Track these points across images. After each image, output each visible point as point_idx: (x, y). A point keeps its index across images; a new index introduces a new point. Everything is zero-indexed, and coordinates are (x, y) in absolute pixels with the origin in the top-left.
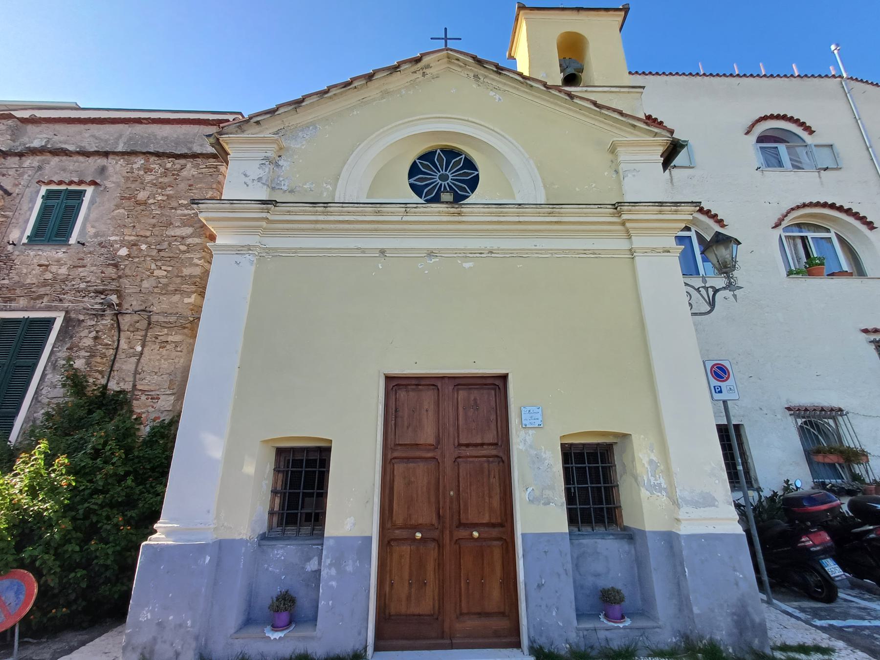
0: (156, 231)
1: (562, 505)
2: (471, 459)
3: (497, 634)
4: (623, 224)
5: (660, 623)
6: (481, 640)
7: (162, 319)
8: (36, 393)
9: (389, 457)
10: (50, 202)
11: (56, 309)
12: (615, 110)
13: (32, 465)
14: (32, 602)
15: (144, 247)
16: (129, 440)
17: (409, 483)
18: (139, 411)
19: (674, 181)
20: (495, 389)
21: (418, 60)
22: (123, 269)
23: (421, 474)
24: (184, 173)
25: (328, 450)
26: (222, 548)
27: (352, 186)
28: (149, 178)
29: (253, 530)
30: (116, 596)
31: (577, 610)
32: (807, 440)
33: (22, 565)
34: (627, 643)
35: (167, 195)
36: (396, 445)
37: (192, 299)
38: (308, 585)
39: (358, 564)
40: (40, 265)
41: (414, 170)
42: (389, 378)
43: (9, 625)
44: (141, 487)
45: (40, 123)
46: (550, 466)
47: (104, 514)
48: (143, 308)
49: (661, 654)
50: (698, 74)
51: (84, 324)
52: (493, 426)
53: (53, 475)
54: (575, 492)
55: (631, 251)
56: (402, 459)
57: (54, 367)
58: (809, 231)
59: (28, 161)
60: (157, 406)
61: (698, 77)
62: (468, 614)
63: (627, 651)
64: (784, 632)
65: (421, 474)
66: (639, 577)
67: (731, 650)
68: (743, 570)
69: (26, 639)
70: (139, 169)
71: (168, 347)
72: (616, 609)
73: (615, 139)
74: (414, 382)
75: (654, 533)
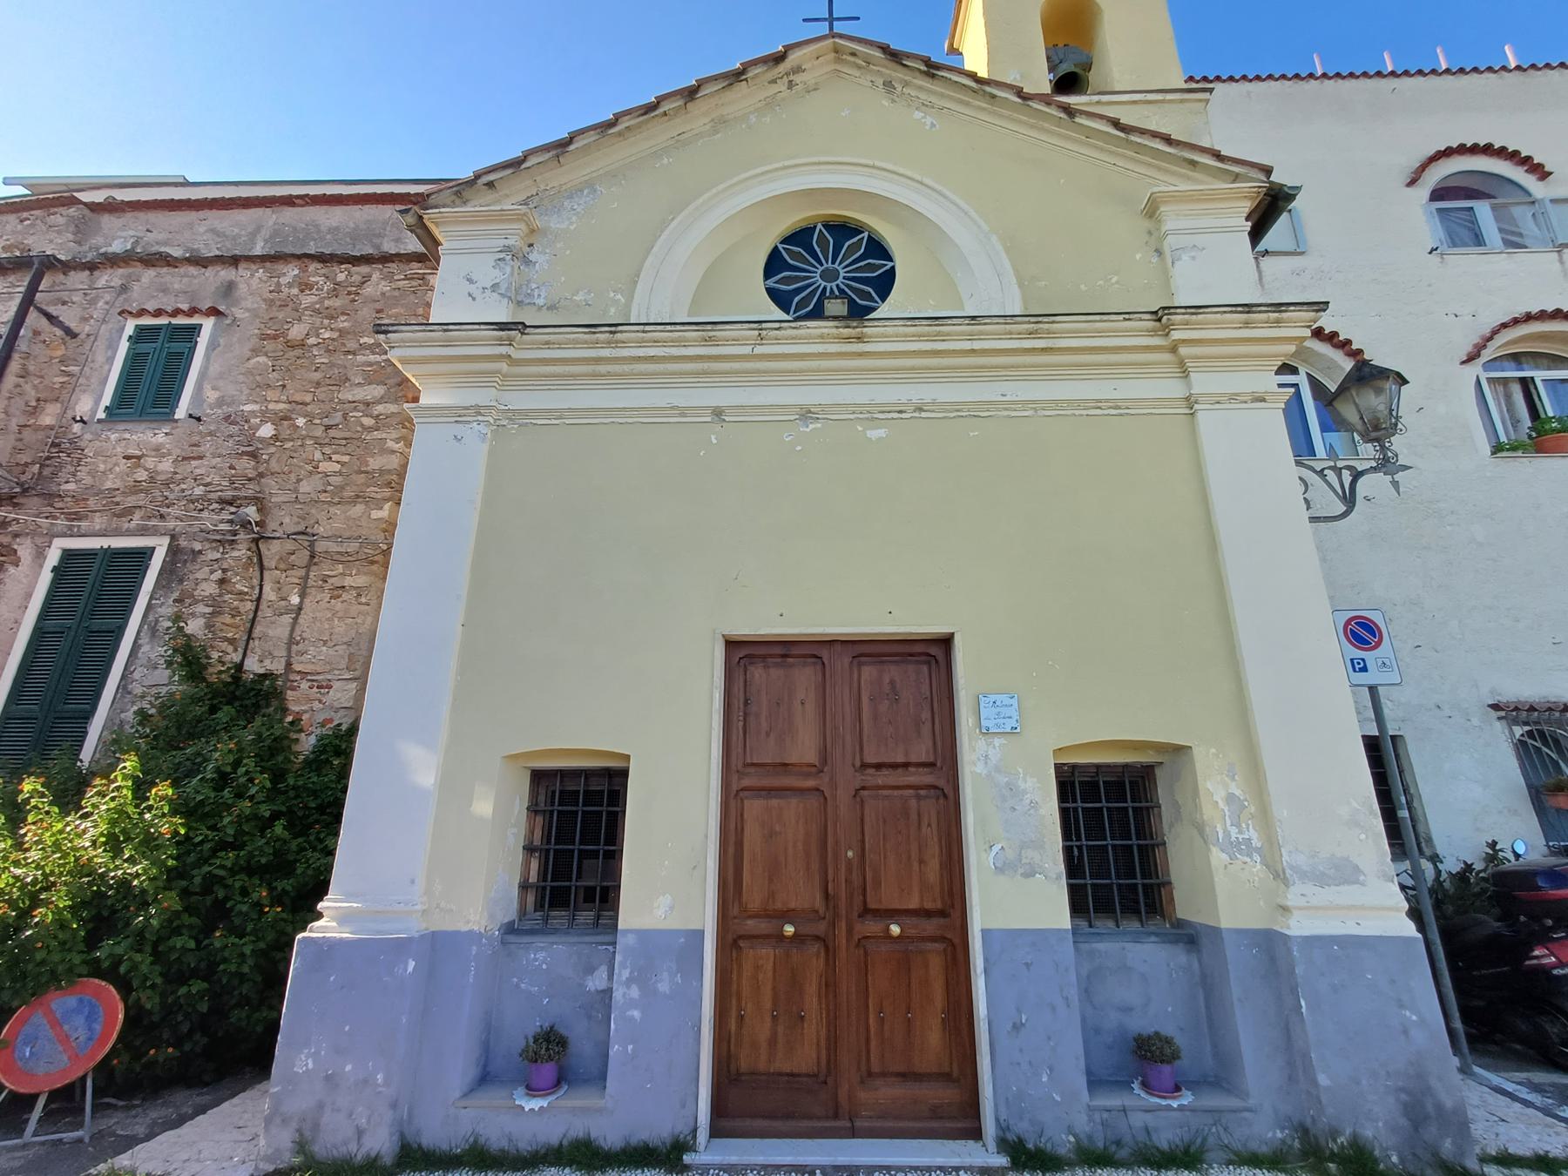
0: (322, 393)
1: (1058, 878)
3: (936, 1113)
4: (1173, 349)
5: (1251, 1102)
6: (911, 1124)
7: (333, 547)
8: (123, 677)
9: (735, 787)
10: (144, 347)
11: (155, 532)
12: (1155, 135)
13: (113, 799)
14: (115, 1036)
15: (301, 422)
16: (280, 758)
20: (929, 663)
21: (779, 58)
22: (267, 462)
23: (792, 815)
24: (368, 290)
25: (624, 774)
26: (438, 948)
27: (663, 293)
28: (307, 300)
29: (491, 917)
30: (259, 1029)
31: (1089, 1073)
32: (1534, 767)
33: (96, 970)
36: (746, 765)
37: (384, 513)
38: (589, 1017)
40: (127, 458)
41: (774, 264)
42: (732, 645)
43: (81, 1074)
44: (300, 840)
45: (123, 211)
46: (1034, 805)
47: (238, 885)
48: (301, 528)
49: (1254, 1161)
50: (1311, 76)
51: (203, 558)
52: (926, 730)
53: (147, 816)
55: (1190, 402)
57: (154, 631)
58: (1537, 368)
59: (105, 278)
62: (884, 1075)
63: (1186, 1152)
64: (1502, 1128)
65: (792, 815)
67: (1395, 1159)
68: (1420, 1008)
69: (107, 1100)
70: (290, 285)
71: (345, 596)
73: (1156, 189)
74: (778, 650)
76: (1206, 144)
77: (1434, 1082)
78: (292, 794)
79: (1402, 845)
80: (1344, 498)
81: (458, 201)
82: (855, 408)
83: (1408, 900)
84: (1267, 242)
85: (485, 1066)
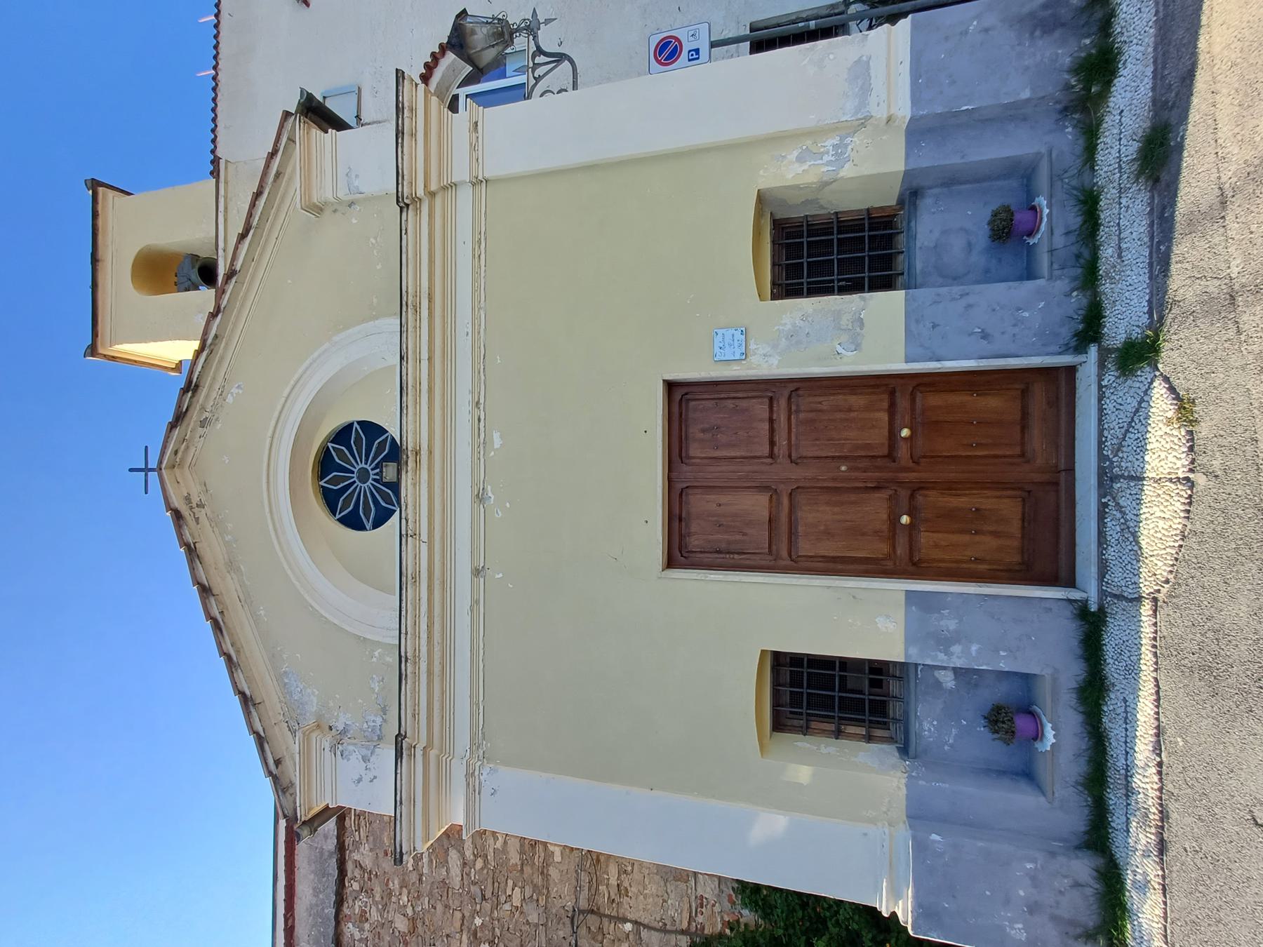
0: (454, 903)
1: (864, 299)
2: (793, 438)
3: (1054, 403)
4: (432, 195)
5: (1044, 150)
7: (584, 894)
12: (253, 205)
15: (478, 921)
17: (828, 534)
18: (720, 926)
19: (379, 118)
20: (688, 400)
21: (178, 516)
23: (813, 515)
24: (368, 863)
25: (777, 656)
27: (374, 616)
28: (374, 915)
29: (894, 767)
31: (1021, 278)
34: (1073, 202)
35: (401, 887)
38: (976, 685)
39: (946, 612)
41: (353, 522)
42: (671, 562)
44: (830, 925)
48: (568, 921)
50: (214, 78)
52: (744, 404)
55: (476, 183)
60: (712, 899)
61: (219, 77)
62: (1023, 444)
63: (1084, 202)
65: (813, 515)
66: (978, 181)
67: (1088, 41)
70: (362, 930)
71: (626, 884)
72: (1021, 217)
73: (299, 206)
75: (907, 156)
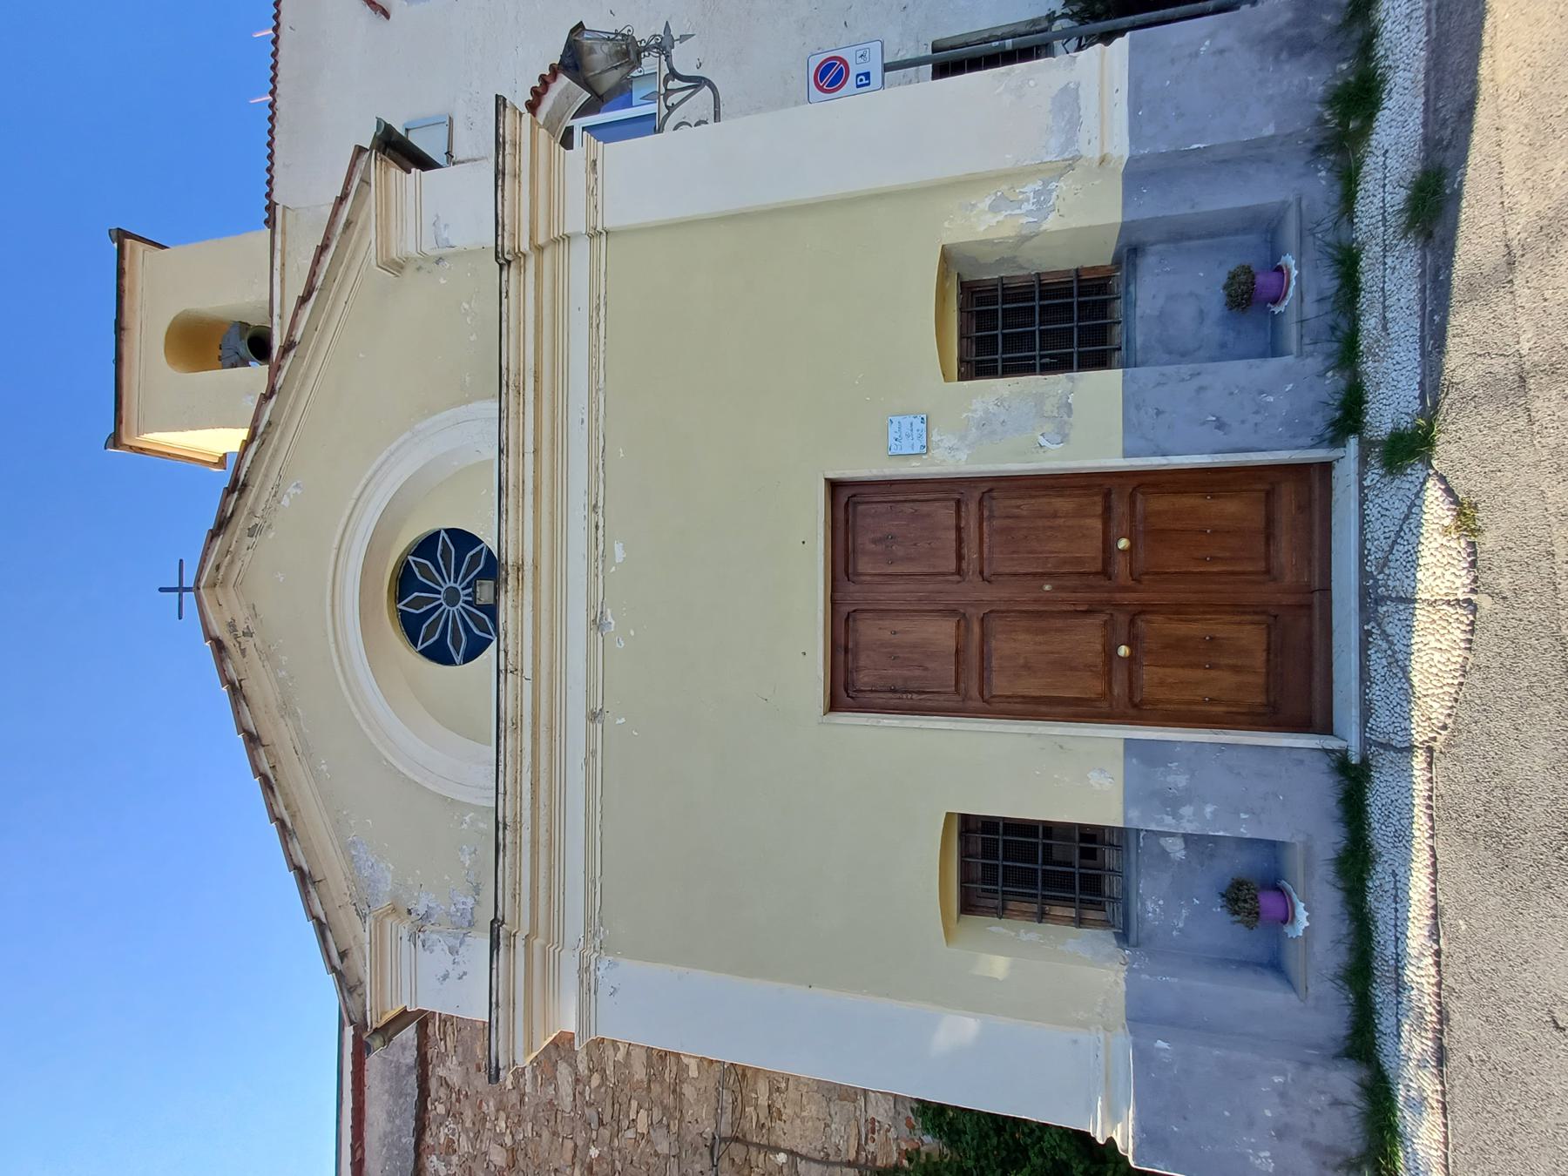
1: (1072, 380)
2: (986, 550)
3: (1305, 507)
4: (540, 249)
5: (1291, 198)
7: (727, 1118)
9: (979, 704)
15: (594, 1152)
18: (895, 1156)
21: (219, 646)
23: (1012, 644)
24: (455, 1080)
25: (965, 819)
26: (1142, 1017)
27: (464, 771)
28: (464, 1145)
34: (1327, 262)
35: (497, 1111)
36: (957, 691)
38: (1212, 856)
41: (438, 654)
42: (834, 705)
46: (1000, 402)
48: (706, 1152)
50: (271, 106)
52: (925, 508)
54: (1050, 356)
56: (983, 680)
60: (886, 1122)
62: (1267, 558)
63: (1341, 262)
65: (1012, 644)
67: (1344, 66)
70: (448, 1164)
71: (779, 1105)
73: (374, 262)
74: (841, 657)
76: (328, 211)
77: (1270, 27)
78: (983, 1163)
79: (1038, 47)
80: (697, 88)
81: (359, 991)
82: (592, 577)
83: (1092, 44)
84: (436, 154)
85: (1261, 965)
